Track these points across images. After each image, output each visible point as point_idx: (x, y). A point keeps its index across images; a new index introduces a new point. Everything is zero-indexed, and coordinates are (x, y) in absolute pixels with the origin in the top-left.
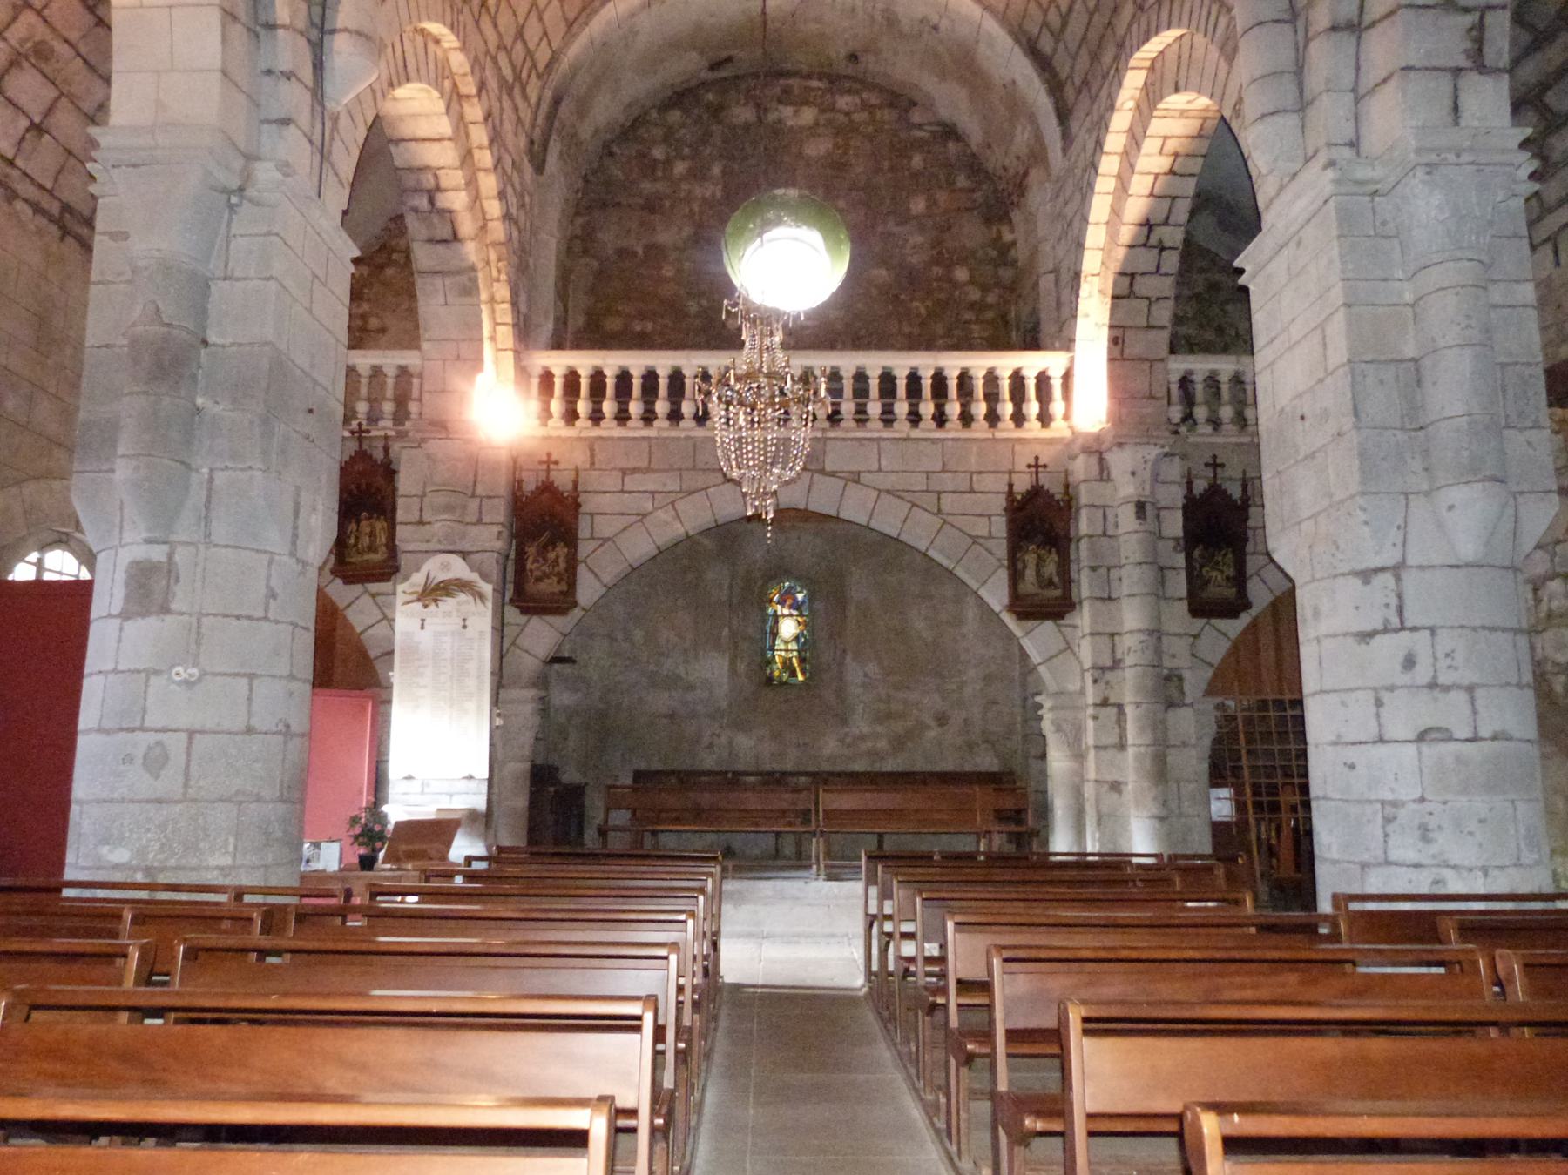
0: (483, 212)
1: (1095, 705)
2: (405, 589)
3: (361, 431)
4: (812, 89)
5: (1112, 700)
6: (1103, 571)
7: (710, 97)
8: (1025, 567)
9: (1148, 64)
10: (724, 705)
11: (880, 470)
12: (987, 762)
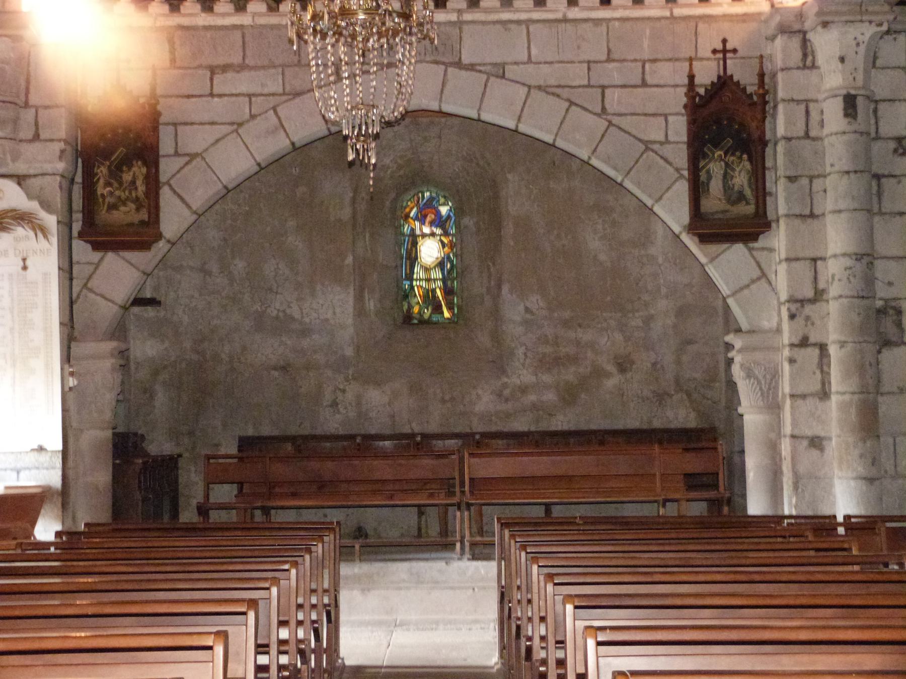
1: (792, 345)
5: (812, 340)
6: (805, 181)
8: (710, 178)
10: (349, 352)
12: (680, 416)
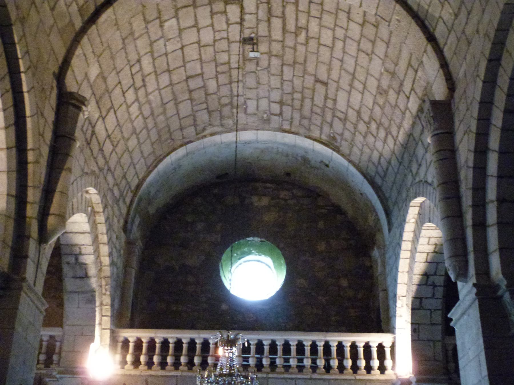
0: (101, 263)
4: (267, 188)
7: (216, 191)
9: (419, 205)
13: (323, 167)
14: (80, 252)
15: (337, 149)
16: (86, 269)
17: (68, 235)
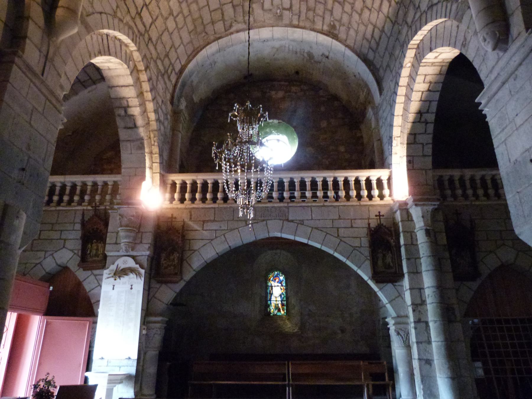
0: (148, 118)
2: (106, 272)
3: (96, 206)
5: (422, 320)
9: (416, 46)
11: (312, 219)
13: (324, 60)
14: (128, 104)
15: (335, 37)
16: (134, 120)
17: (115, 88)
